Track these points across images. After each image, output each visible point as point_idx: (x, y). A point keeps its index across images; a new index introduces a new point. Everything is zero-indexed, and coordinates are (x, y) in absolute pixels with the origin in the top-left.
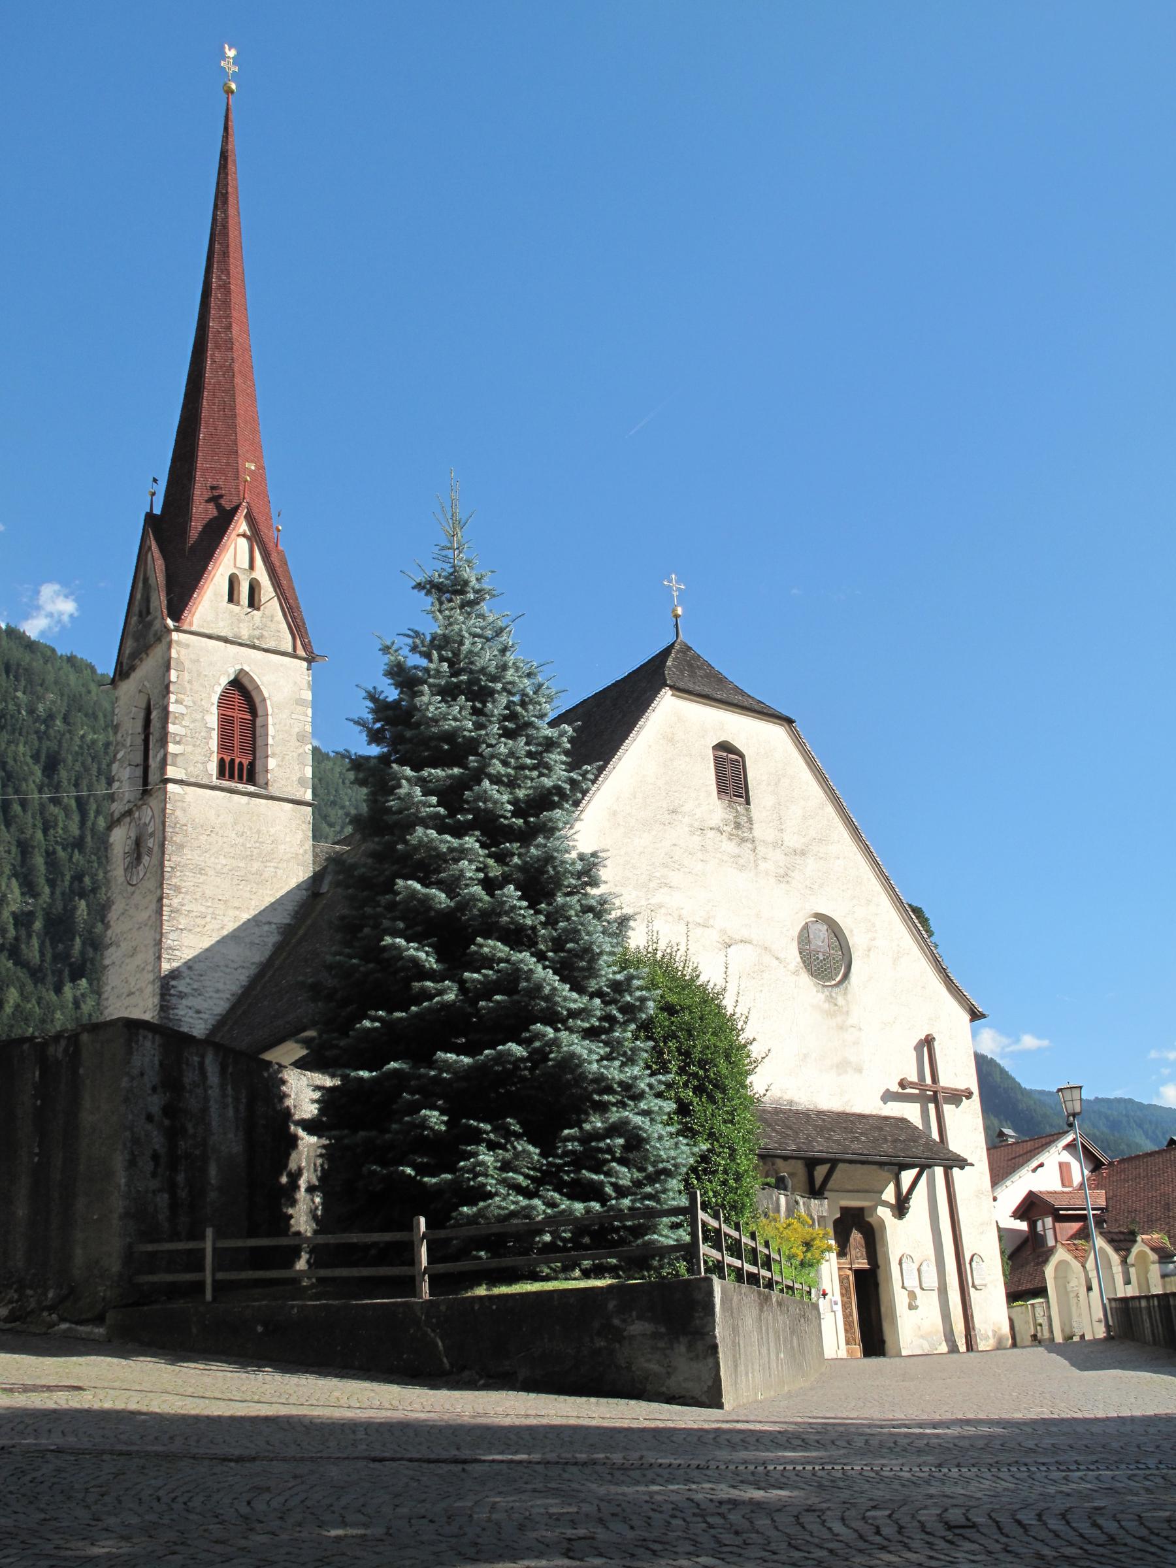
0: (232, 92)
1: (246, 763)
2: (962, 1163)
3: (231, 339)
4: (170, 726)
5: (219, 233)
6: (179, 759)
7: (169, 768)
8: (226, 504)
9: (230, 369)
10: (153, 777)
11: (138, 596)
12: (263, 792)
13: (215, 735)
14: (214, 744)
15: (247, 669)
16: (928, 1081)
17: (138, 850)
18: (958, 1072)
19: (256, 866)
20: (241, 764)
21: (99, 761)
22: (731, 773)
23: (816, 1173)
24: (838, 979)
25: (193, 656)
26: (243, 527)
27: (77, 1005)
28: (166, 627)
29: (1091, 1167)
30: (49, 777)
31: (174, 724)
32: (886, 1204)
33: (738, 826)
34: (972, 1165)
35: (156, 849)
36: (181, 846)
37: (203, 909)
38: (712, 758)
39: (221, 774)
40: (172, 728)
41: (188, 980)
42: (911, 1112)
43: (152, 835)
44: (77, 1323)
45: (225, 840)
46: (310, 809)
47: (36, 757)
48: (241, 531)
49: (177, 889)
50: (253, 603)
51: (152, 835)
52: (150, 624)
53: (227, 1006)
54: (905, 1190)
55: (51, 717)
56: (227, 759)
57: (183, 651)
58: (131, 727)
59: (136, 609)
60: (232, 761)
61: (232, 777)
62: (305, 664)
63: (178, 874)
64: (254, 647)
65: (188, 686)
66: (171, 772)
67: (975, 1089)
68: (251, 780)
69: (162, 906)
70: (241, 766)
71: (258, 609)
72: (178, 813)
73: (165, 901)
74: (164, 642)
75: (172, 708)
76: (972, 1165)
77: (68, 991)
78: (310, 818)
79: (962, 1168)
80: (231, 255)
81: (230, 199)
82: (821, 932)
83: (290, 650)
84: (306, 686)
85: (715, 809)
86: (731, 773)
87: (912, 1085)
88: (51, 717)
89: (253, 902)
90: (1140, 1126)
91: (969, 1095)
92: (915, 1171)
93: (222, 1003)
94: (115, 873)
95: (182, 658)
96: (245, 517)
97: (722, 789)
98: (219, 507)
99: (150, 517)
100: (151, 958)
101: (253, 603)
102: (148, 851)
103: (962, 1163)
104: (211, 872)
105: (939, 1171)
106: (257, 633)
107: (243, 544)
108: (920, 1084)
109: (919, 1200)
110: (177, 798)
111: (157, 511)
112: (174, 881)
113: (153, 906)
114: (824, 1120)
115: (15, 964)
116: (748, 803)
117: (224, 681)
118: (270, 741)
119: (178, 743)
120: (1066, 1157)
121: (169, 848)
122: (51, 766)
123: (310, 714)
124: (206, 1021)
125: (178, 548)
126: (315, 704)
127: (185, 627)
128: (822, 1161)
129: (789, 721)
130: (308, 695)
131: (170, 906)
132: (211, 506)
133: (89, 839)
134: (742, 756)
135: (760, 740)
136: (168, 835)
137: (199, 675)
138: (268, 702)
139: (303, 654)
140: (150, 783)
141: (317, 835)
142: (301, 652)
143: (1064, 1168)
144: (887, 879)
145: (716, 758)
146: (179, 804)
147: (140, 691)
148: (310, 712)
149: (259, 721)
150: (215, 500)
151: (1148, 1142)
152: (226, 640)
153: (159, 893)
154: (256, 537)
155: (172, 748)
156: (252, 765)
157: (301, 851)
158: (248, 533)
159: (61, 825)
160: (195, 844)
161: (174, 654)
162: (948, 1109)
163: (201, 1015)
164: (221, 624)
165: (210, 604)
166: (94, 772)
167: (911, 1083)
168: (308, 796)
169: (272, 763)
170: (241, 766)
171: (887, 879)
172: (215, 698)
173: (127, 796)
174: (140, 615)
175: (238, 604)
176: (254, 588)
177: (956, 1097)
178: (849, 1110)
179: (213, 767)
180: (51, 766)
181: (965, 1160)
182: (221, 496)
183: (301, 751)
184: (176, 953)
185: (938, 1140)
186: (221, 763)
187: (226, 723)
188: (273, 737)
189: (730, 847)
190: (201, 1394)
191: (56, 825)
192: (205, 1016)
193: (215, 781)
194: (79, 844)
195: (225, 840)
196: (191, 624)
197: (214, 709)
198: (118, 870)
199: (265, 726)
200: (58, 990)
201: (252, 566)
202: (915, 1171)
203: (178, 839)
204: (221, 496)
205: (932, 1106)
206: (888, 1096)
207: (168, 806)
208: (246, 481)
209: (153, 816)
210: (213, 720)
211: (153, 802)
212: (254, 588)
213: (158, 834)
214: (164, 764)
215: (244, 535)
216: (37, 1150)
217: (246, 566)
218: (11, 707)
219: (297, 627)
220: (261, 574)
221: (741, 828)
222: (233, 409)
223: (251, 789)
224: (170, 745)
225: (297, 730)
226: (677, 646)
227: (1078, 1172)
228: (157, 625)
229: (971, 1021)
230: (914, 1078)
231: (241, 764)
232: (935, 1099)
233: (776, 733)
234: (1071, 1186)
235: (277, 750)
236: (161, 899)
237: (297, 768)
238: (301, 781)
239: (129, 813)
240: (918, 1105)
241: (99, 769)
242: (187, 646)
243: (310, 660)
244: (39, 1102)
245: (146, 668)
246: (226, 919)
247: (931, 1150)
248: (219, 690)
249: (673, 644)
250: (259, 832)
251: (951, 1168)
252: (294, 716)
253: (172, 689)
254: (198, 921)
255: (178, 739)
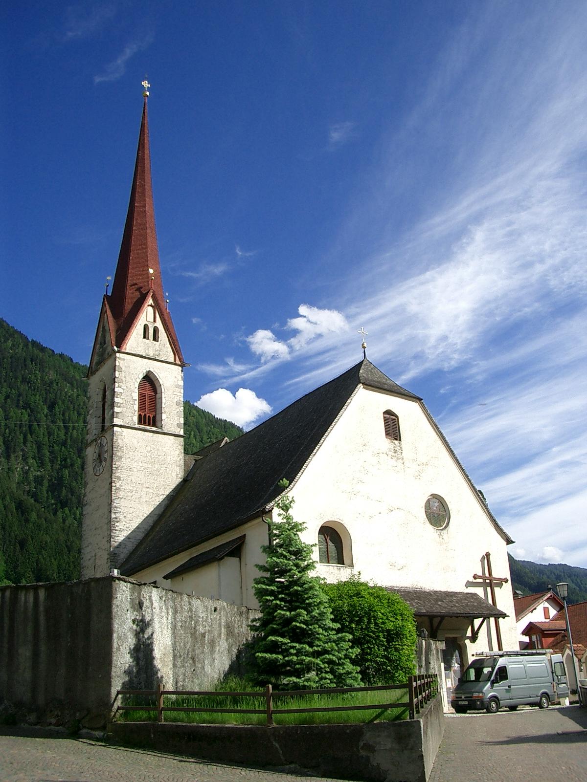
0: (147, 96)
1: (151, 416)
2: (504, 616)
3: (145, 211)
4: (115, 398)
5: (140, 162)
6: (120, 415)
7: (115, 419)
8: (144, 291)
9: (145, 225)
10: (107, 424)
11: (100, 335)
12: (160, 430)
13: (137, 402)
14: (136, 407)
15: (152, 370)
16: (487, 575)
17: (100, 458)
18: (502, 570)
19: (157, 466)
20: (149, 416)
21: (82, 414)
22: (392, 426)
23: (434, 622)
24: (444, 526)
25: (126, 364)
26: (150, 301)
27: (64, 521)
28: (113, 350)
29: (558, 609)
30: (51, 411)
31: (117, 397)
32: (468, 638)
33: (395, 451)
34: (508, 616)
35: (108, 458)
36: (121, 457)
37: (131, 488)
38: (383, 418)
39: (140, 422)
40: (116, 400)
41: (124, 523)
42: (479, 591)
43: (106, 451)
44: (92, 729)
45: (142, 454)
46: (182, 439)
47: (45, 402)
48: (150, 304)
49: (119, 478)
50: (155, 338)
51: (106, 451)
52: (106, 349)
53: (143, 535)
54: (476, 628)
55: (51, 383)
56: (143, 414)
57: (122, 362)
58: (95, 397)
59: (99, 342)
60: (145, 415)
61: (145, 424)
62: (180, 368)
63: (119, 471)
64: (156, 360)
65: (124, 379)
66: (116, 421)
67: (509, 578)
68: (154, 425)
69: (112, 486)
70: (150, 417)
71: (158, 341)
72: (119, 441)
73: (113, 484)
74: (113, 357)
75: (116, 390)
76: (508, 616)
77: (60, 514)
78: (182, 443)
79: (504, 618)
80: (146, 172)
81: (146, 146)
82: (436, 504)
83: (173, 361)
84: (180, 378)
85: (386, 443)
86: (392, 426)
87: (480, 577)
88: (51, 383)
89: (155, 485)
90: (570, 577)
91: (506, 581)
92: (481, 619)
93: (140, 534)
94: (88, 469)
95: (121, 366)
96: (152, 297)
97: (388, 434)
98: (141, 293)
99: (106, 296)
100: (107, 512)
101: (155, 338)
102: (106, 457)
103: (504, 616)
104: (135, 470)
105: (492, 620)
106: (157, 353)
107: (150, 310)
108: (483, 577)
109: (482, 634)
110: (118, 433)
111: (109, 294)
112: (117, 474)
113: (107, 486)
114: (437, 596)
115: (35, 501)
116: (400, 440)
117: (141, 376)
118: (163, 406)
119: (119, 407)
120: (547, 605)
121: (115, 458)
122: (51, 407)
123: (183, 392)
124: (133, 543)
125: (120, 312)
126: (185, 388)
127: (123, 350)
128: (437, 616)
129: (420, 400)
130: (181, 383)
131: (115, 486)
132: (137, 293)
133: (69, 440)
134: (397, 417)
135: (409, 413)
136: (114, 452)
137: (130, 373)
138: (162, 386)
139: (180, 363)
140: (106, 426)
141: (186, 452)
142: (178, 362)
143: (546, 610)
144: (467, 476)
145: (385, 419)
146: (120, 437)
147: (101, 381)
148: (182, 391)
149: (158, 396)
150: (139, 289)
151: (573, 585)
152: (142, 357)
153: (110, 481)
154: (157, 307)
155: (116, 410)
156: (154, 417)
157: (178, 460)
158: (153, 304)
159: (56, 433)
160: (128, 456)
161: (117, 364)
162: (496, 589)
163: (131, 540)
164: (140, 349)
165: (135, 340)
166: (72, 408)
167: (479, 576)
168: (182, 433)
169: (164, 416)
170: (150, 417)
171: (467, 476)
172: (137, 385)
173: (95, 432)
174: (101, 344)
175: (148, 339)
176: (156, 330)
177: (500, 582)
178: (449, 590)
179: (136, 419)
180: (51, 407)
181: (506, 614)
182: (141, 288)
183: (178, 410)
184: (118, 509)
185: (492, 604)
186: (140, 416)
187: (142, 397)
188: (165, 404)
189: (393, 462)
190: (149, 756)
191: (54, 433)
192: (133, 541)
193: (137, 426)
194: (64, 444)
195: (142, 454)
196: (125, 349)
197: (137, 390)
198: (89, 468)
199: (161, 398)
200: (55, 514)
201: (155, 321)
202: (481, 619)
203: (119, 454)
204: (141, 288)
205: (489, 589)
206: (469, 584)
207: (114, 438)
208: (152, 279)
209: (107, 443)
210: (136, 396)
211: (107, 435)
212: (156, 330)
213: (110, 451)
214: (112, 417)
215: (151, 306)
216: (69, 640)
217: (152, 321)
218: (33, 377)
219: (176, 350)
220: (159, 324)
221: (397, 453)
222: (146, 245)
223: (154, 429)
224: (115, 408)
225: (176, 400)
226: (364, 363)
227: (553, 612)
228: (109, 349)
229: (507, 544)
230: (480, 574)
231: (149, 416)
232: (491, 585)
233: (414, 406)
234: (549, 619)
235: (166, 410)
236: (111, 483)
237: (176, 419)
238: (178, 425)
239: (96, 440)
240: (482, 588)
241: (74, 407)
242: (124, 360)
243: (182, 366)
244: (70, 616)
245: (104, 370)
246: (142, 493)
247: (489, 610)
248: (139, 381)
249: (363, 361)
250: (158, 450)
251: (499, 618)
252: (174, 393)
253: (116, 380)
254: (129, 494)
255: (119, 405)
